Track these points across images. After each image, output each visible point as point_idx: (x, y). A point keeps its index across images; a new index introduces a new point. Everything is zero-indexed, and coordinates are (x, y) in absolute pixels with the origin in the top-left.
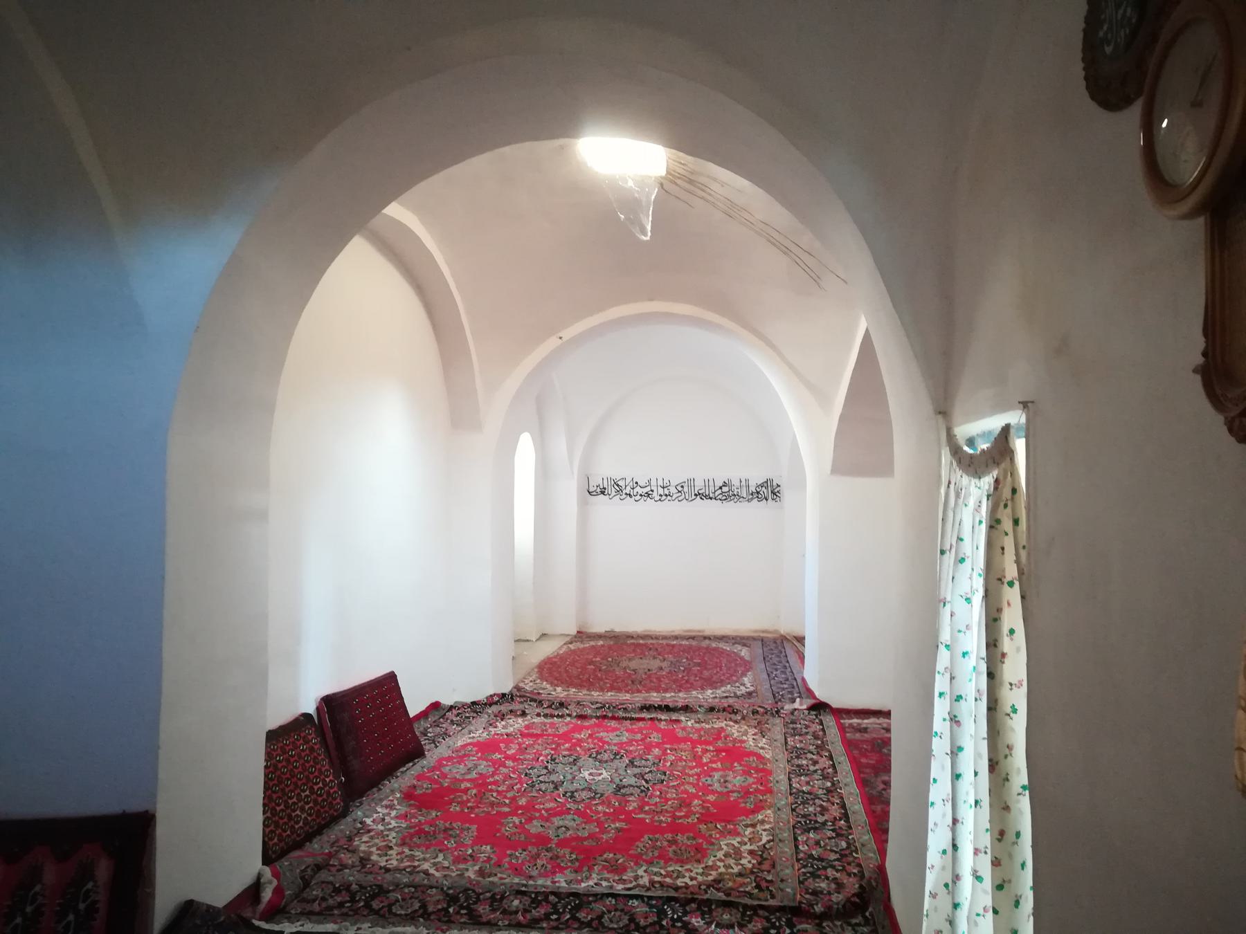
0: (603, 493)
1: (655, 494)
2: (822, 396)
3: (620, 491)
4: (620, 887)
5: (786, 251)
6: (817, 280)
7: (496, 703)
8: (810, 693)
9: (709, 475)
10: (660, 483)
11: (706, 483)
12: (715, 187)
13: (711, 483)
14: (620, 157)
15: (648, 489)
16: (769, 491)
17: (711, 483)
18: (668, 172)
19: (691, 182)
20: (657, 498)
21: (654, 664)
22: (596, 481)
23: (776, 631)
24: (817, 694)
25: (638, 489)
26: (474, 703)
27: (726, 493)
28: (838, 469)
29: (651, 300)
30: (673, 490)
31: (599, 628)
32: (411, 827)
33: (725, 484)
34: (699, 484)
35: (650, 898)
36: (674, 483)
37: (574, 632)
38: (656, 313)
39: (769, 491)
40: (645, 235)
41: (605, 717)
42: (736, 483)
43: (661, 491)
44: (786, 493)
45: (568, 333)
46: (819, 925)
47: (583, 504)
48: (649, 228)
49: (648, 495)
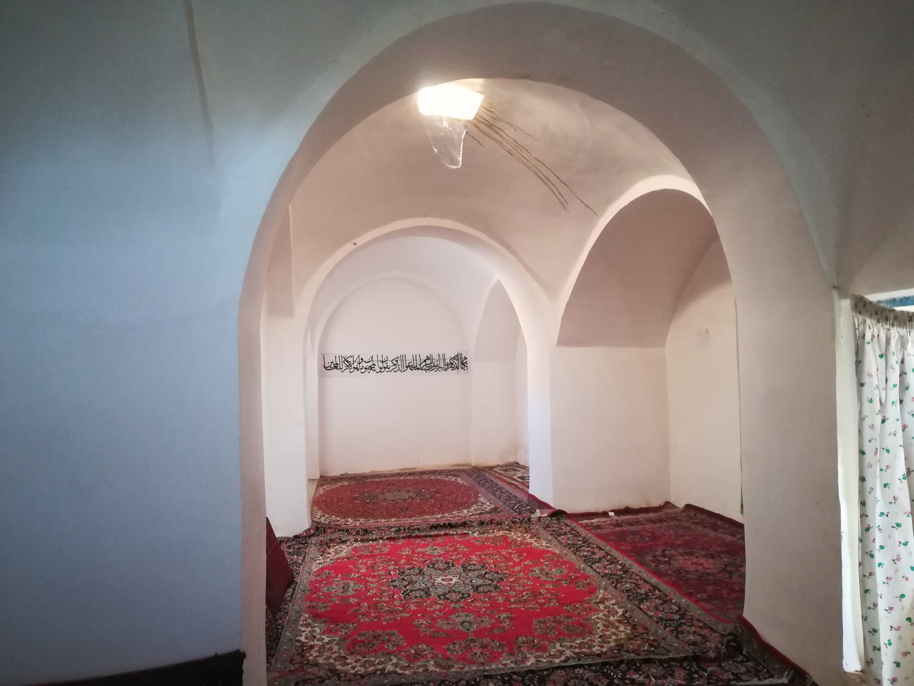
0: (336, 367)
1: (376, 367)
2: (550, 288)
3: (349, 366)
4: (557, 661)
5: (545, 181)
6: (564, 204)
7: (313, 535)
8: (543, 505)
9: (416, 352)
10: (380, 359)
11: (414, 357)
12: (510, 132)
13: (418, 358)
14: (449, 101)
15: (371, 363)
16: (459, 363)
17: (418, 358)
18: (476, 118)
19: (491, 126)
20: (378, 370)
21: (404, 495)
22: (330, 359)
23: (467, 465)
24: (552, 505)
25: (363, 364)
26: (296, 537)
27: (429, 365)
28: (566, 339)
29: (425, 216)
30: (390, 364)
31: (336, 472)
32: (345, 639)
33: (428, 358)
34: (409, 358)
35: (589, 665)
36: (390, 359)
37: (318, 477)
38: (439, 228)
39: (459, 363)
40: (456, 164)
41: (410, 537)
42: (436, 357)
43: (381, 365)
44: (472, 363)
45: (361, 240)
46: (720, 666)
47: (321, 376)
48: (460, 159)
49: (371, 368)
